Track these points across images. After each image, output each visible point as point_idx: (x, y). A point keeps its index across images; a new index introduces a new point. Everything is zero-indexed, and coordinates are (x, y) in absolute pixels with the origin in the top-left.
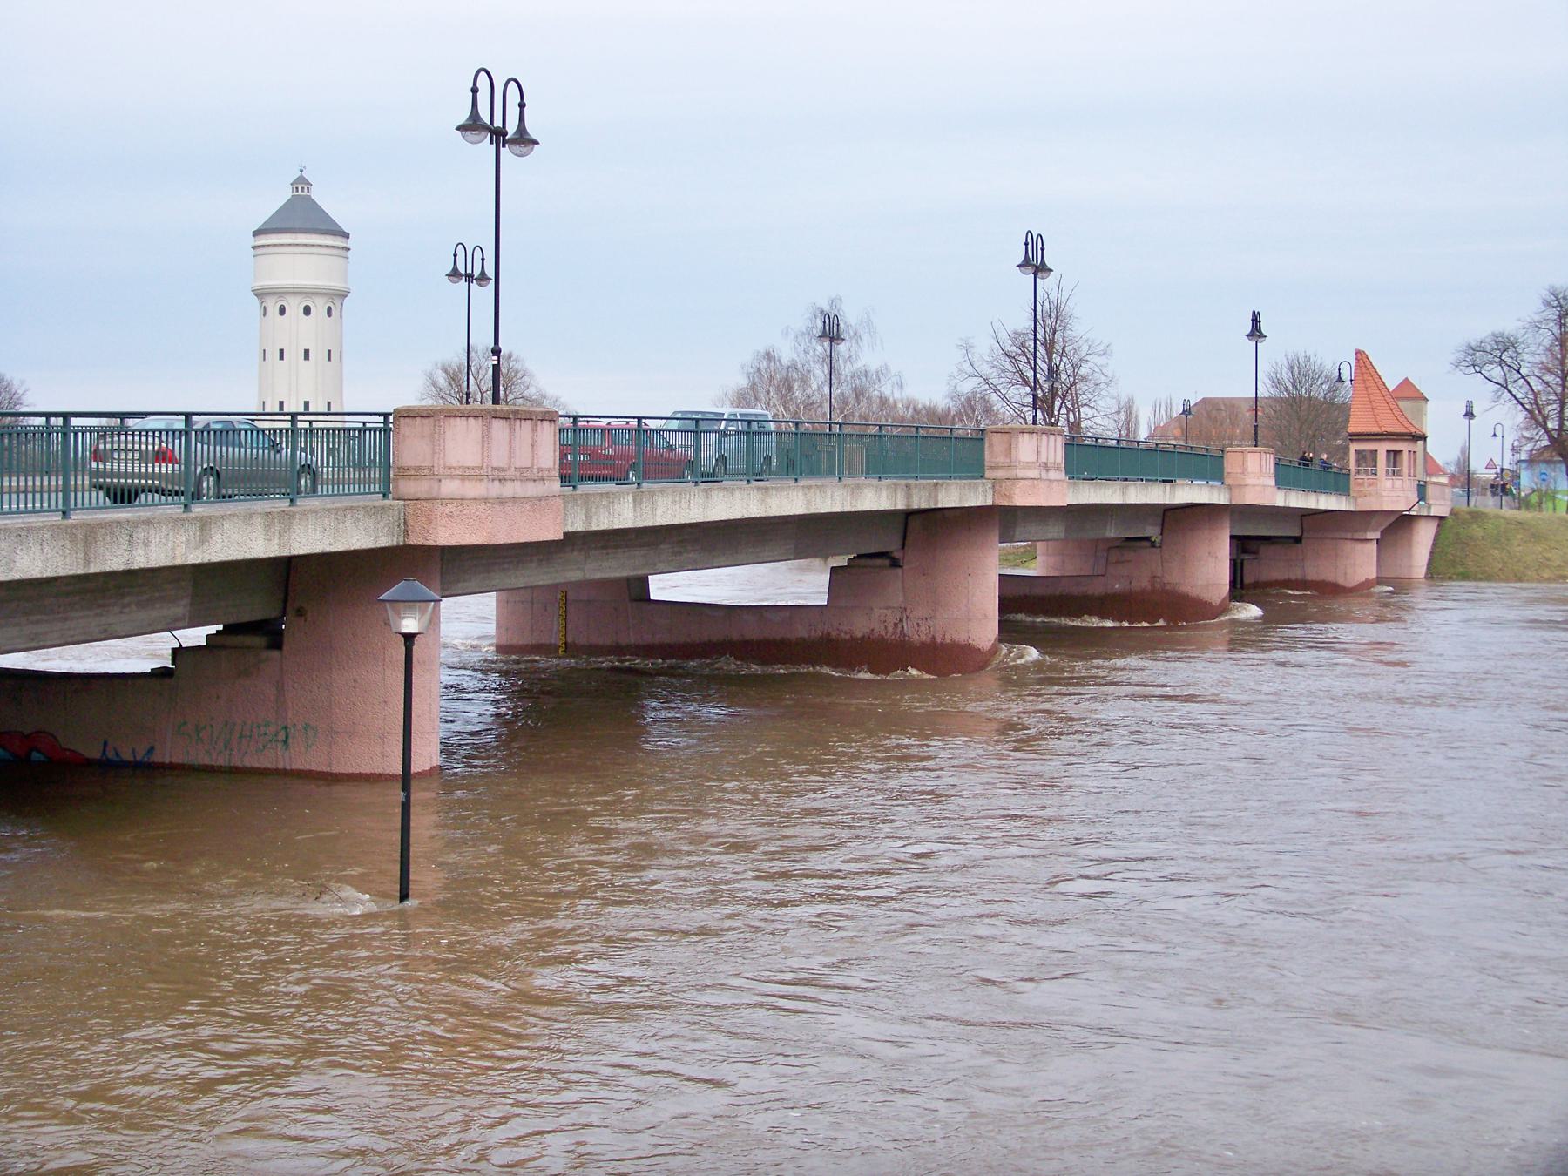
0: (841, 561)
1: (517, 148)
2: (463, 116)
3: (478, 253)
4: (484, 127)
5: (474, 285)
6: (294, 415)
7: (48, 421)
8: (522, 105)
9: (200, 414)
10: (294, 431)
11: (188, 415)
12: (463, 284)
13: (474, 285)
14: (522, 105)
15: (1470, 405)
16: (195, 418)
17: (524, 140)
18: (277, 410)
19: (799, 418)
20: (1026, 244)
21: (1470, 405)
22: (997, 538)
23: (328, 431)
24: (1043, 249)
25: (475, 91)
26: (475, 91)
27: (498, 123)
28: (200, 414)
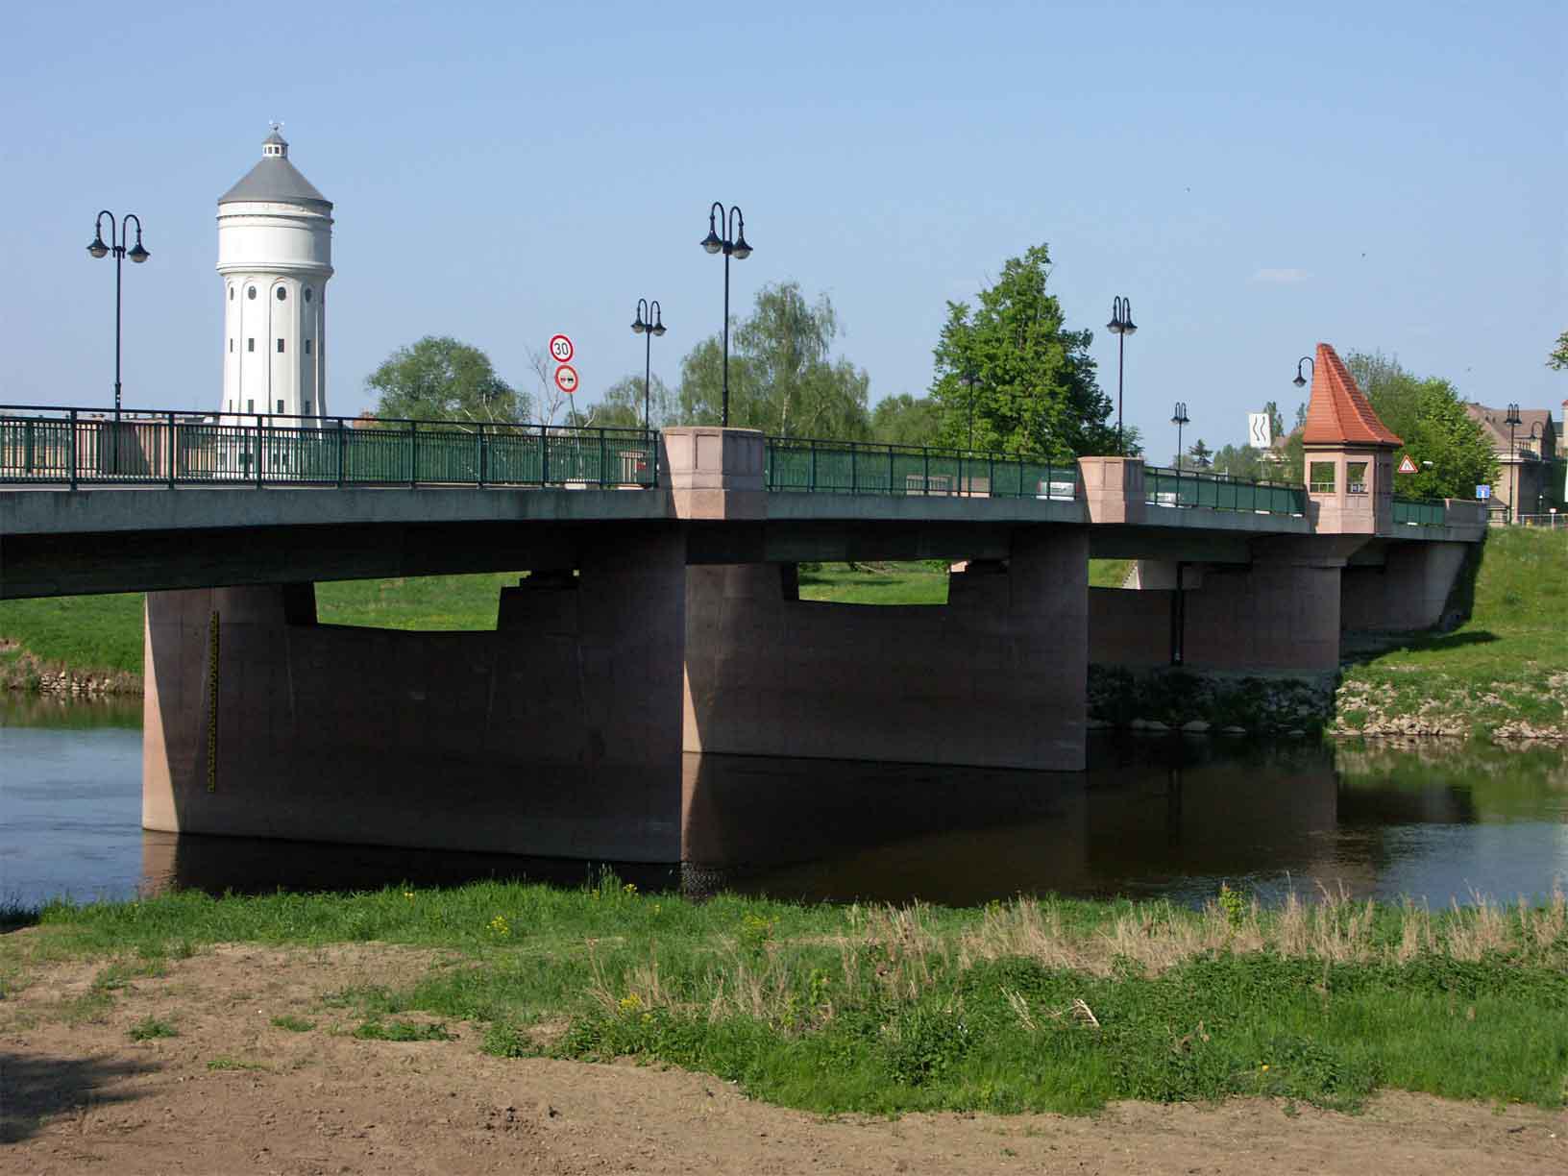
0: (959, 567)
1: (738, 253)
2: (705, 234)
3: (131, 224)
4: (720, 242)
5: (127, 261)
6: (260, 417)
7: (544, 431)
8: (741, 224)
9: (349, 419)
10: (543, 437)
11: (172, 414)
12: (110, 258)
13: (652, 335)
14: (741, 224)
15: (1122, 305)
16: (418, 425)
17: (743, 248)
18: (245, 410)
19: (485, 416)
20: (1115, 308)
21: (1122, 305)
22: (1086, 551)
23: (30, 429)
24: (1129, 310)
25: (713, 218)
26: (713, 218)
27: (727, 239)
28: (349, 419)
